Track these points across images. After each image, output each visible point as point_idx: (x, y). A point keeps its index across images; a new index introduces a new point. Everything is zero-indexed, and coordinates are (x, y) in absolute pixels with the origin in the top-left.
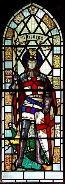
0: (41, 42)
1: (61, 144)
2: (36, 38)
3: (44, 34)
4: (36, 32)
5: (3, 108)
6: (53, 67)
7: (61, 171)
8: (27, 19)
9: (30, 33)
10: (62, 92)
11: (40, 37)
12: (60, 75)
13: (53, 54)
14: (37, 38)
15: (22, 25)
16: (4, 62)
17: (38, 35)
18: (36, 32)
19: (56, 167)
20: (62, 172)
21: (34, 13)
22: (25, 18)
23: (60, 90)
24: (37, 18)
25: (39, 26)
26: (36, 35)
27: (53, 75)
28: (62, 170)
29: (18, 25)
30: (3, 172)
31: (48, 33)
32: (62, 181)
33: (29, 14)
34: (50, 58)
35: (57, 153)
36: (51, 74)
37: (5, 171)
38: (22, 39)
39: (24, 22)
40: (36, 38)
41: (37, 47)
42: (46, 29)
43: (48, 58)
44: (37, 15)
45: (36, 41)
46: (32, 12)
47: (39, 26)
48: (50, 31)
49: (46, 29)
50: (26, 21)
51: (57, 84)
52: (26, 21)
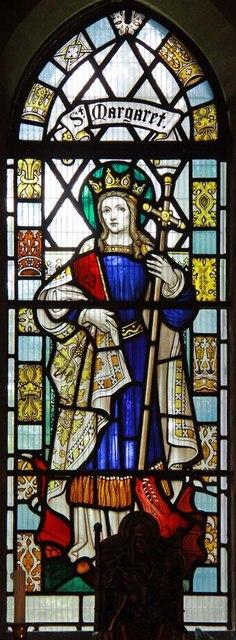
0: (152, 132)
2: (119, 117)
4: (136, 96)
5: (10, 515)
7: (219, 593)
8: (108, 49)
9: (112, 97)
11: (132, 111)
13: (192, 180)
14: (123, 113)
15: (87, 70)
16: (14, 509)
17: (144, 107)
20: (224, 599)
22: (96, 51)
23: (216, 305)
24: (141, 48)
26: (135, 106)
27: (190, 250)
28: (224, 589)
29: (68, 74)
31: (176, 100)
32: (224, 165)
36: (186, 245)
38: (77, 122)
39: (94, 63)
40: (119, 117)
41: (91, 162)
42: (169, 88)
45: (131, 129)
48: (183, 92)
49: (169, 88)
50: (100, 58)
52: (100, 58)
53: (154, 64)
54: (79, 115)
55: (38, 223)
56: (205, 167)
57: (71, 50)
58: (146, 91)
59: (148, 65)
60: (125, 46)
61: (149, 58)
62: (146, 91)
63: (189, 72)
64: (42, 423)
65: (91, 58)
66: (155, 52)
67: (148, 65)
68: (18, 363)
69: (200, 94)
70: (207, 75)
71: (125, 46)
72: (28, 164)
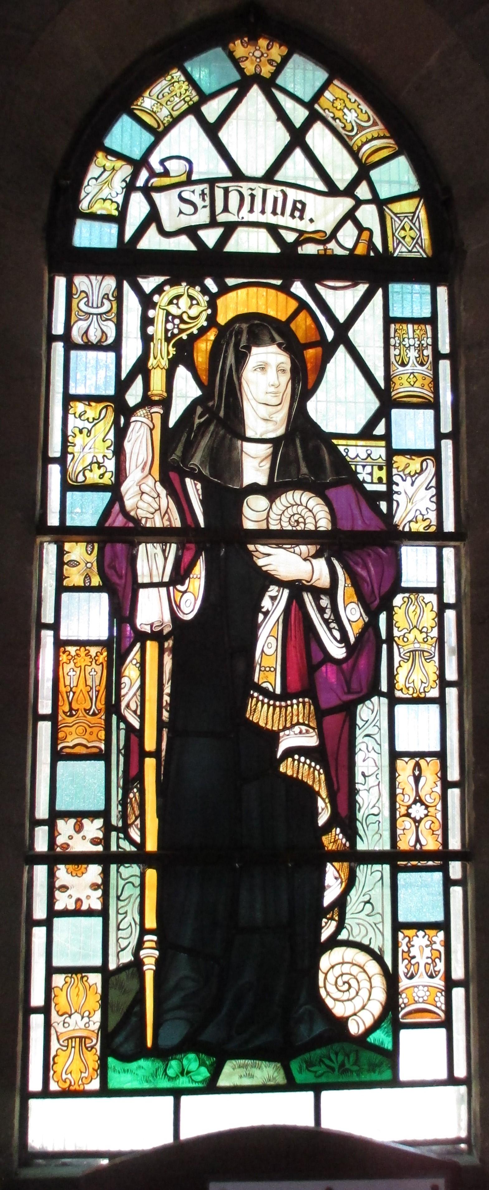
1: (439, 436)
3: (333, 191)
5: (39, 934)
6: (387, 401)
7: (452, 1080)
8: (233, 93)
9: (238, 175)
10: (449, 553)
12: (436, 747)
13: (388, 321)
16: (48, 923)
18: (278, 177)
19: (422, 1052)
21: (266, 71)
22: (205, 98)
23: (436, 537)
24: (281, 97)
25: (298, 138)
27: (387, 437)
28: (460, 1072)
30: (33, 1103)
32: (442, 292)
33: (236, 77)
34: (367, 333)
35: (421, 637)
36: (380, 430)
37: (46, 1093)
43: (353, 334)
44: (279, 81)
45: (273, 230)
46: (249, 68)
47: (298, 138)
48: (364, 173)
51: (415, 502)
52: (212, 110)
53: (308, 124)
54: (196, 199)
55: (111, 391)
56: (411, 299)
57: (162, 97)
58: (297, 167)
59: (298, 125)
60: (255, 93)
61: (298, 115)
62: (297, 167)
63: (374, 138)
64: (104, 756)
65: (195, 110)
66: (309, 105)
67: (298, 125)
68: (60, 644)
69: (397, 176)
70: (407, 139)
71: (255, 93)
72: (96, 287)
